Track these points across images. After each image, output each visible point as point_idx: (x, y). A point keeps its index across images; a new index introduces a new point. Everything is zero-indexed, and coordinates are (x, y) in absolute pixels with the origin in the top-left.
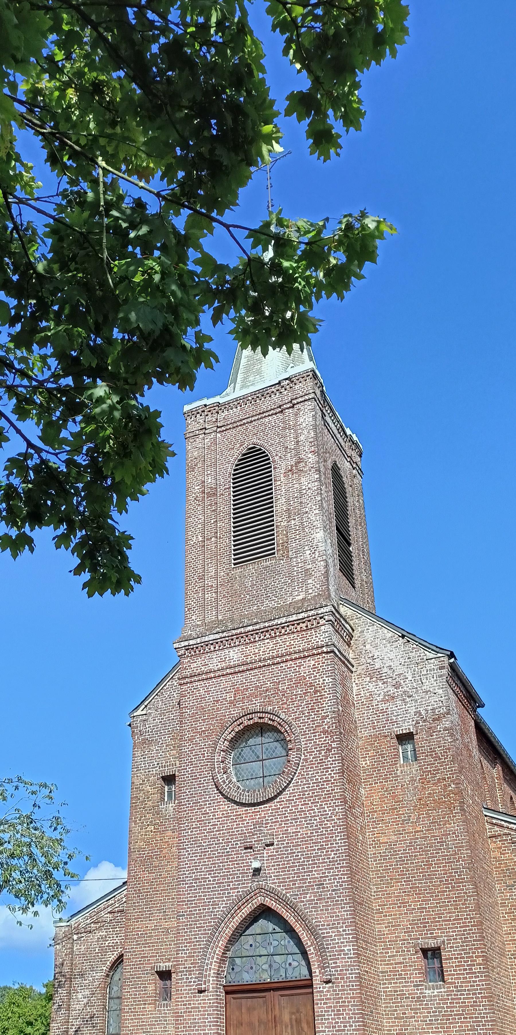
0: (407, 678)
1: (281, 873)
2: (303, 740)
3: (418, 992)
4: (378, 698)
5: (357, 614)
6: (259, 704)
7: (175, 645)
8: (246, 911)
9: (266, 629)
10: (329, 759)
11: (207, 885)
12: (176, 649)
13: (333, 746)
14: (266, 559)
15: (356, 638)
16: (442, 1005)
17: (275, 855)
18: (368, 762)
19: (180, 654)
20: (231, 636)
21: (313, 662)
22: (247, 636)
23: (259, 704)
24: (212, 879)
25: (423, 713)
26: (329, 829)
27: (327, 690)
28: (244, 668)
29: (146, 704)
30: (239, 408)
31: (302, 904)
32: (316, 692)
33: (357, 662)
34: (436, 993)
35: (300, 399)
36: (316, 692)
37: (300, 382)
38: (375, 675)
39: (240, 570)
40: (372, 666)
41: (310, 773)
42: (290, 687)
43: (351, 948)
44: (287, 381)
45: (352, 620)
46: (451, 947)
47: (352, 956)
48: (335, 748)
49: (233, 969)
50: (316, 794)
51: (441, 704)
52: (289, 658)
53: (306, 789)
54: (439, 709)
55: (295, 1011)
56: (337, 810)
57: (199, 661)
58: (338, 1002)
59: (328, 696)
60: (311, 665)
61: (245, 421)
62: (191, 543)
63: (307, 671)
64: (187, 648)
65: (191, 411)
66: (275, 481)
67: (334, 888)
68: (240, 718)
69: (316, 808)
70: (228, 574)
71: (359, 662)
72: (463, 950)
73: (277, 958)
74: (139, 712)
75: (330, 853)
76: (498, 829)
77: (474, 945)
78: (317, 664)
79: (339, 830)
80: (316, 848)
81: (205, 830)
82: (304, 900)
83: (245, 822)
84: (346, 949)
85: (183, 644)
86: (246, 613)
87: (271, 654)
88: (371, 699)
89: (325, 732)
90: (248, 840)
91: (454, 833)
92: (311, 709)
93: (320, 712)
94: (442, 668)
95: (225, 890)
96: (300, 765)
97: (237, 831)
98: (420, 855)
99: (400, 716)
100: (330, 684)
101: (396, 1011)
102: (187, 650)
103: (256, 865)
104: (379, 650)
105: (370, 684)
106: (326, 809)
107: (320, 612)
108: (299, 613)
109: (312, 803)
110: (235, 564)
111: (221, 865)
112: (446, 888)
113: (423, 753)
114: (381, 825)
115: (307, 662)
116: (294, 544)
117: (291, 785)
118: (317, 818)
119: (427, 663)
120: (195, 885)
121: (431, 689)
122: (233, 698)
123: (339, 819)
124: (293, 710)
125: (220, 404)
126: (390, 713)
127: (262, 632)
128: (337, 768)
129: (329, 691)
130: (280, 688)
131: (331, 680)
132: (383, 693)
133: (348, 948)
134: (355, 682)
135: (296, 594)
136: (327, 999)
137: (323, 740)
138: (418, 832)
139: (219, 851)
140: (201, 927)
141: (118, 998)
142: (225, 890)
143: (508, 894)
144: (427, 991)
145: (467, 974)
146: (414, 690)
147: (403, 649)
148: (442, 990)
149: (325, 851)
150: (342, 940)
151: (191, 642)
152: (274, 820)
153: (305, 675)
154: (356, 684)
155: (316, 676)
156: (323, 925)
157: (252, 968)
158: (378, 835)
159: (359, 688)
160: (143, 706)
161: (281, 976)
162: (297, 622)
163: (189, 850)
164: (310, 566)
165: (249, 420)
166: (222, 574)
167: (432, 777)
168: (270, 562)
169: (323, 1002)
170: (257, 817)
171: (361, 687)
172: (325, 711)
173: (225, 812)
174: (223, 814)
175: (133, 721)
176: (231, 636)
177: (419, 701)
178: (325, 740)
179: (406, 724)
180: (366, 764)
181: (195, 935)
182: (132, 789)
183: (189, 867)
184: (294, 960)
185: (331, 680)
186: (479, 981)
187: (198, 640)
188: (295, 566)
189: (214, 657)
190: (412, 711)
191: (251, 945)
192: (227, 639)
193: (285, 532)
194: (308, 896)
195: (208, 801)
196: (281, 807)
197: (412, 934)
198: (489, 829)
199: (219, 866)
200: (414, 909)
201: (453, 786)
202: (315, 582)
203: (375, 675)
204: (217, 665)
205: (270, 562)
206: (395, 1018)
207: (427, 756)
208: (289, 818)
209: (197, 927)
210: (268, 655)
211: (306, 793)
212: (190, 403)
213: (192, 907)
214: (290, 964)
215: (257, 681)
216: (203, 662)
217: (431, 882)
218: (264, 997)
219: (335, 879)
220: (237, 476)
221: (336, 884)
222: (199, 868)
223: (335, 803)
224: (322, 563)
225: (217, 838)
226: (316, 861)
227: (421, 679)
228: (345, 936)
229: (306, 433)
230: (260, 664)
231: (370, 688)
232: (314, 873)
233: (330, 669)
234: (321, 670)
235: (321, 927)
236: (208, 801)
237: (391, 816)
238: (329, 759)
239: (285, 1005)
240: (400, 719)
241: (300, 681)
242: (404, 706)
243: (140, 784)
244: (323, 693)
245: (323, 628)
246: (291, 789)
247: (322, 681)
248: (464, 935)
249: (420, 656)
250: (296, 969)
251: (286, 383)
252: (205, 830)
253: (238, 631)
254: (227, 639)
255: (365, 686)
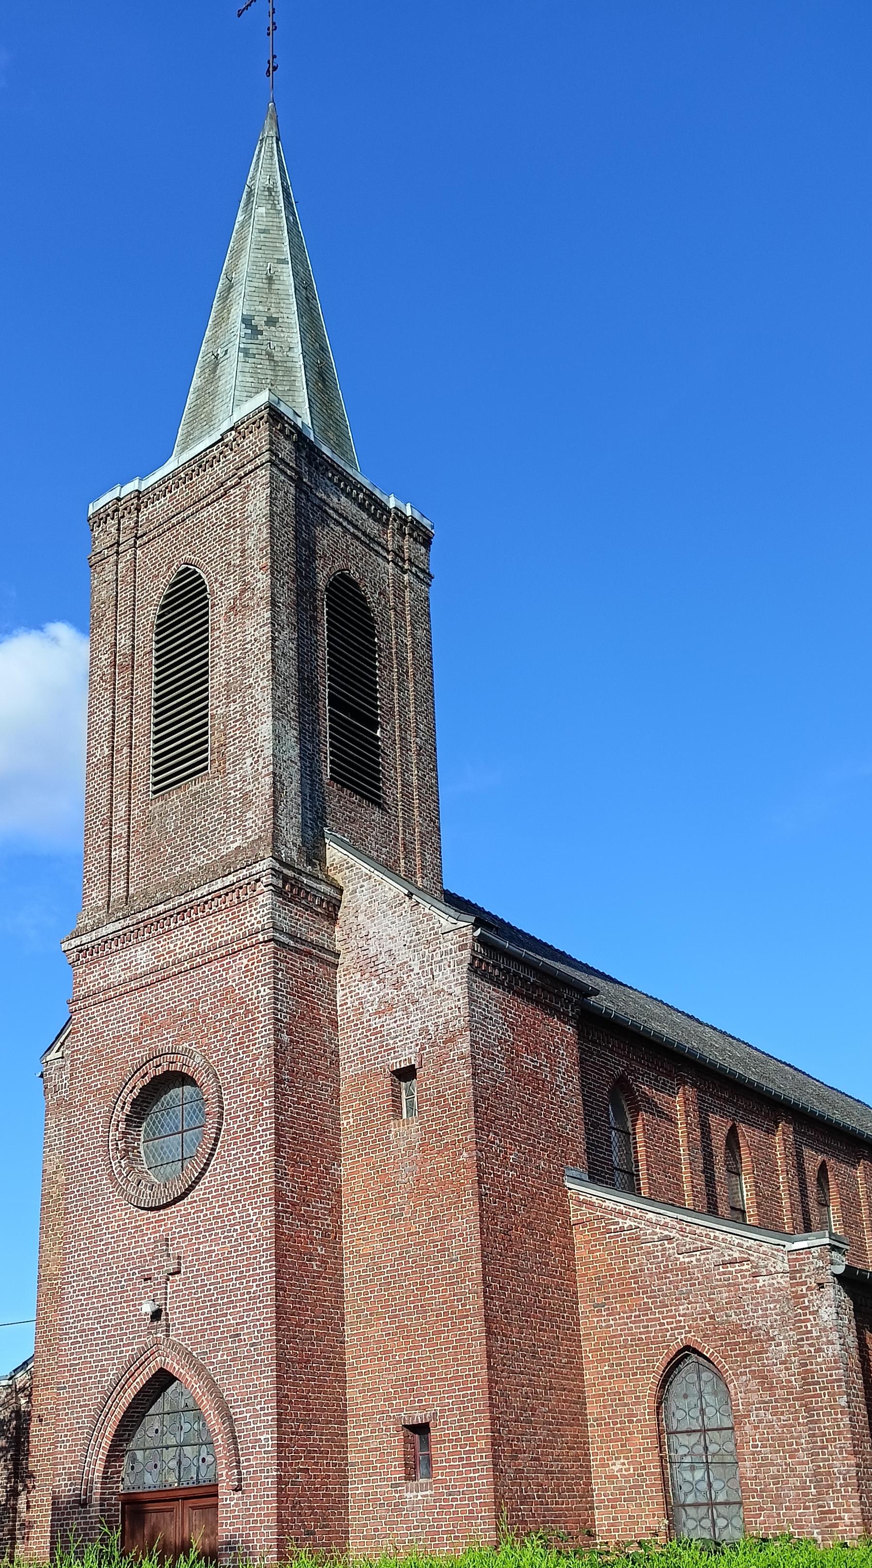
0: (412, 970)
1: (187, 1319)
2: (226, 1097)
3: (397, 1495)
4: (370, 1008)
5: (349, 860)
6: (171, 1040)
7: (63, 945)
9: (168, 914)
10: (259, 1128)
11: (95, 1339)
12: (65, 951)
13: (265, 1105)
14: (191, 781)
15: (345, 904)
16: (426, 1517)
17: (181, 1290)
18: (351, 1120)
19: (71, 960)
20: (137, 924)
21: (245, 961)
22: (158, 922)
23: (171, 1040)
24: (101, 1330)
25: (432, 1029)
26: (252, 1245)
27: (262, 1009)
28: (153, 978)
29: (61, 1040)
30: (168, 495)
31: (211, 1367)
32: (247, 1012)
33: (344, 947)
34: (419, 1498)
35: (250, 467)
36: (247, 1012)
37: (251, 432)
38: (370, 967)
39: (160, 803)
40: (365, 953)
41: (233, 1152)
42: (214, 1008)
43: (269, 1436)
44: (233, 432)
45: (341, 871)
46: (446, 1423)
47: (270, 1449)
48: (267, 1108)
49: (133, 1468)
50: (238, 1187)
51: (458, 1014)
52: (212, 956)
53: (226, 1180)
54: (454, 1023)
55: (209, 1532)
56: (264, 1214)
57: (97, 972)
58: (248, 1522)
59: (263, 1019)
60: (243, 966)
61: (174, 521)
62: (95, 760)
63: (237, 978)
65: (97, 514)
66: (213, 630)
67: (254, 1341)
68: (144, 1065)
69: (237, 1211)
70: (144, 811)
71: (347, 946)
72: (461, 1427)
73: (188, 1450)
74: (53, 1055)
75: (251, 1284)
76: (587, 1211)
77: (475, 1419)
78: (250, 963)
79: (265, 1247)
80: (234, 1276)
81: (95, 1252)
82: (214, 1360)
83: (146, 1238)
84: (262, 1438)
86: (166, 879)
87: (191, 951)
88: (361, 1010)
89: (255, 1082)
90: (147, 1268)
91: (461, 1235)
92: (239, 1044)
93: (251, 1048)
94: (462, 948)
95: (116, 1347)
96: (221, 1139)
97: (136, 1253)
98: (414, 1273)
99: (400, 1038)
100: (267, 998)
101: (365, 1525)
102: (81, 951)
103: (147, 1308)
104: (376, 922)
105: (361, 985)
106: (251, 1212)
107: (254, 871)
108: (226, 876)
109: (232, 1203)
110: (155, 792)
111: (113, 1307)
112: (444, 1326)
113: (427, 1100)
114: (362, 1226)
115: (238, 962)
116: (232, 748)
117: (207, 1174)
118: (238, 1227)
119: (442, 940)
120: (81, 1340)
121: (445, 987)
122: (138, 1032)
123: (265, 1228)
124: (216, 1047)
125: (140, 492)
126: (385, 1033)
127: (178, 913)
128: (268, 1143)
129: (265, 1010)
130: (200, 1010)
131: (268, 991)
132: (377, 999)
133: (265, 1436)
134: (340, 981)
135: (232, 839)
136: (234, 1517)
137: (252, 1095)
138: (412, 1234)
139: (112, 1285)
140: (86, 1406)
142: (116, 1347)
143: (595, 1320)
144: (408, 1495)
145: (464, 1466)
146: (421, 990)
147: (410, 919)
148: (428, 1493)
149: (244, 1281)
150: (259, 1425)
151: (85, 939)
152: (183, 1233)
153: (234, 984)
154: (342, 986)
155: (249, 985)
156: (236, 1401)
157: (156, 1466)
158: (359, 1242)
159: (345, 992)
160: (59, 1044)
161: (192, 1478)
162: (225, 891)
163: (75, 1284)
164: (250, 787)
165: (180, 517)
166: (136, 812)
167: (437, 1142)
168: (201, 784)
169: (229, 1522)
170: (161, 1229)
171: (348, 990)
172: (257, 1046)
173: (121, 1223)
174: (119, 1226)
175: (46, 1071)
176: (137, 924)
177: (427, 1010)
178: (255, 1096)
179: (407, 1052)
180: (348, 1123)
181: (77, 1418)
182: (43, 1181)
183: (74, 1312)
184: (208, 1454)
185: (268, 991)
186: (479, 1478)
187: (94, 935)
188: (231, 789)
189: (116, 961)
190: (417, 1027)
191: (157, 1431)
192: (131, 928)
193: (222, 727)
194: (219, 1354)
195: (101, 1205)
196: (193, 1211)
197: (394, 1402)
198: (575, 1210)
199: (110, 1310)
200: (399, 1362)
201: (465, 1154)
202: (256, 816)
203: (370, 967)
204: (120, 976)
205: (201, 784)
206: (365, 1537)
207: (432, 1105)
208: (202, 1229)
209: (81, 1407)
210: (186, 954)
211: (226, 1187)
212: (97, 498)
213: (76, 1375)
214: (204, 1460)
215: (170, 999)
216: (102, 972)
217: (424, 1318)
218: (171, 1510)
219: (255, 1326)
220: (163, 628)
221: (256, 1334)
222: (85, 1313)
223: (262, 1202)
224: (267, 778)
225: (110, 1264)
226: (233, 1298)
227: (432, 969)
228: (262, 1418)
229: (255, 532)
230: (175, 970)
231: (360, 992)
232: (229, 1317)
233: (268, 970)
234: (256, 974)
235: (233, 1404)
236: (101, 1205)
237: (377, 1209)
238: (259, 1128)
239: (197, 1523)
240: (399, 1044)
241: (226, 996)
242: (406, 1021)
243: (54, 1173)
244: (257, 1015)
245: (260, 898)
246: (206, 1181)
247: (255, 995)
248: (463, 1402)
249: (433, 929)
250: (211, 1467)
251: (231, 438)
252: (95, 1252)
253: (145, 914)
254: (131, 928)
255: (353, 989)
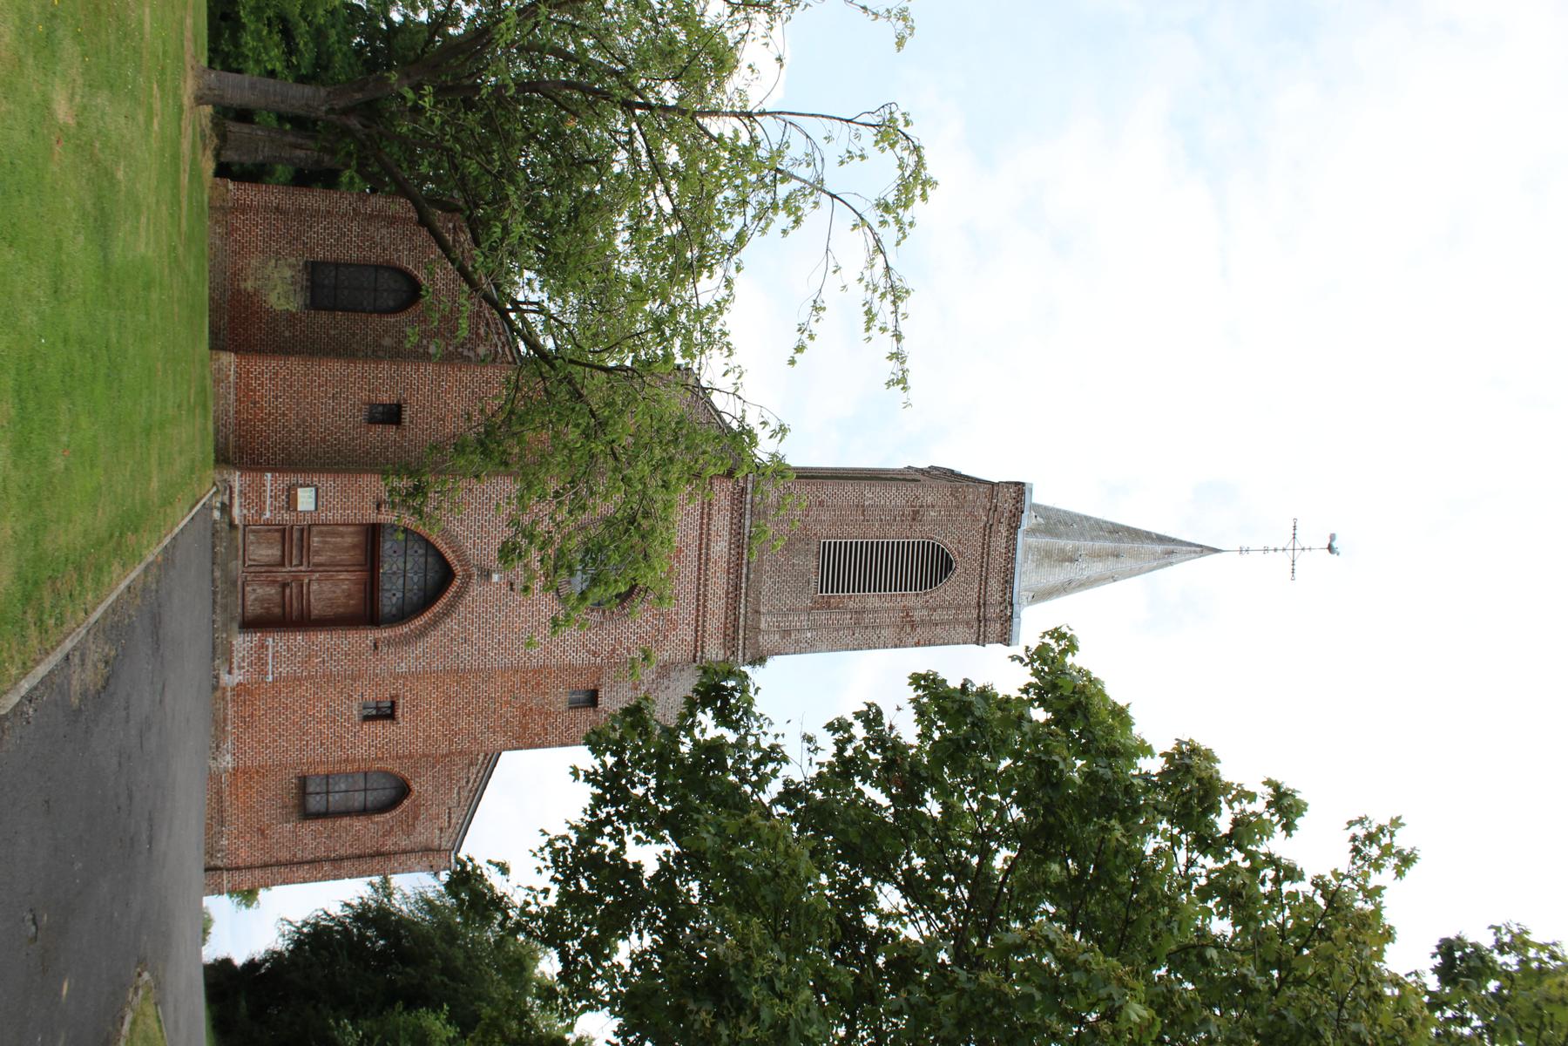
8: (450, 556)
64: (744, 490)
73: (401, 581)
85: (750, 486)
89: (614, 650)
141: (216, 868)
